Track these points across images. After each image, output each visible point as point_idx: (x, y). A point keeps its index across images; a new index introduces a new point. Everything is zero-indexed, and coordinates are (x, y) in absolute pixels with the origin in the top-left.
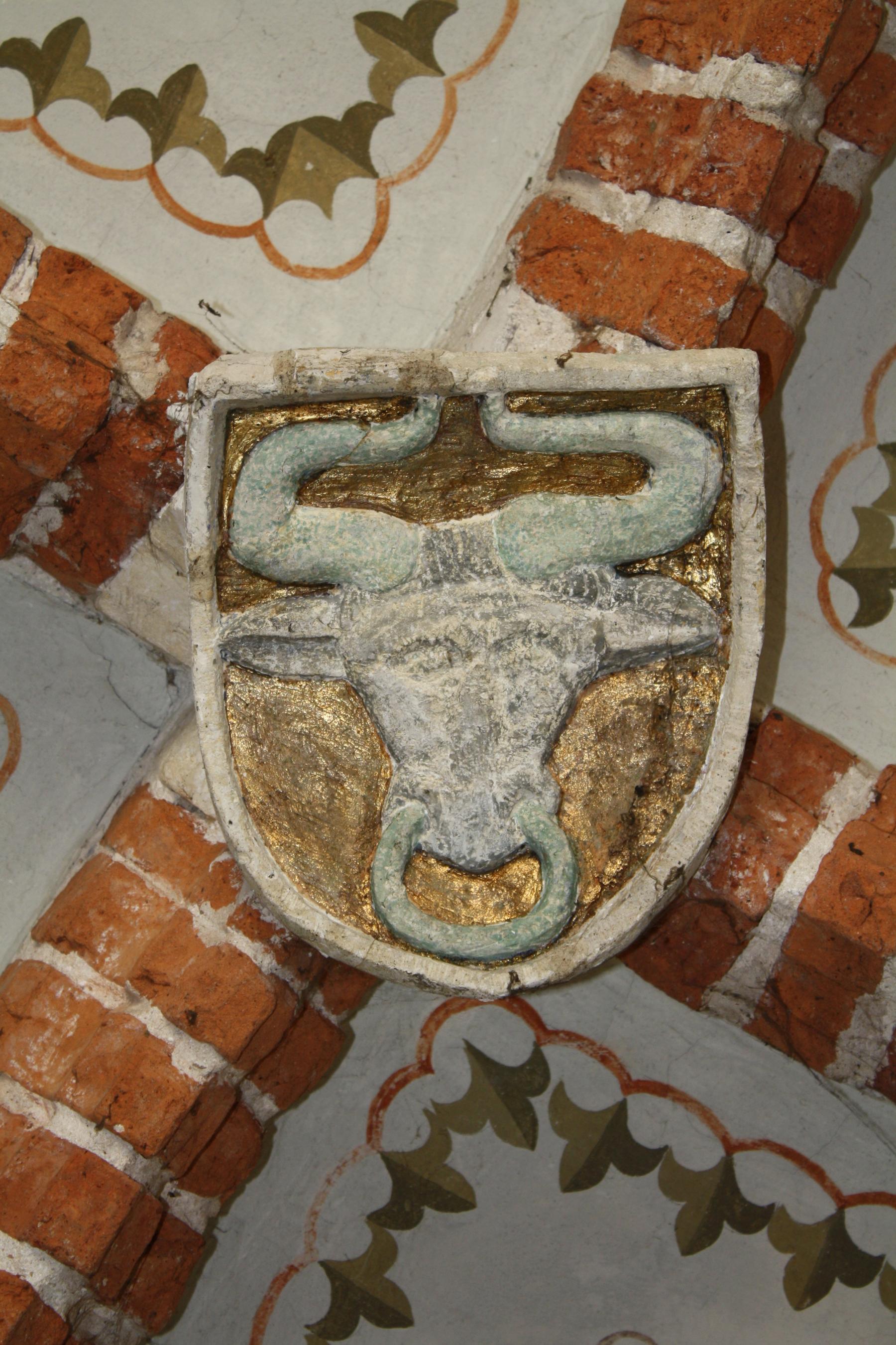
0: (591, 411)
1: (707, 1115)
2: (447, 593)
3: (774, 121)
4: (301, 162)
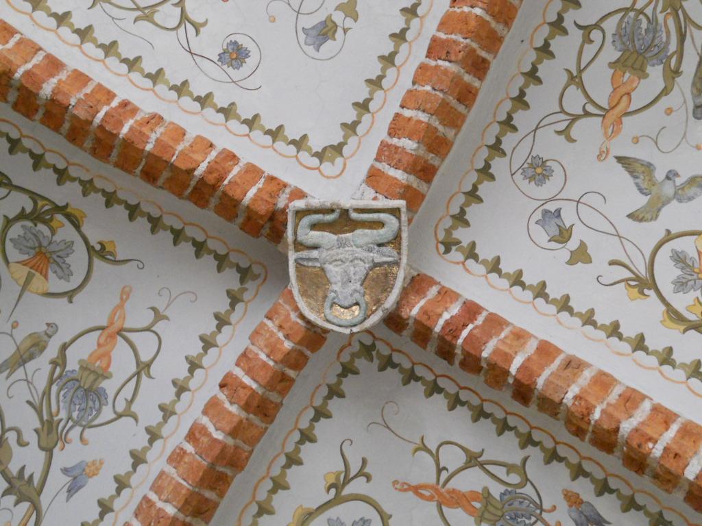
0: (371, 213)
2: (341, 250)
3: (413, 152)
4: (328, 154)
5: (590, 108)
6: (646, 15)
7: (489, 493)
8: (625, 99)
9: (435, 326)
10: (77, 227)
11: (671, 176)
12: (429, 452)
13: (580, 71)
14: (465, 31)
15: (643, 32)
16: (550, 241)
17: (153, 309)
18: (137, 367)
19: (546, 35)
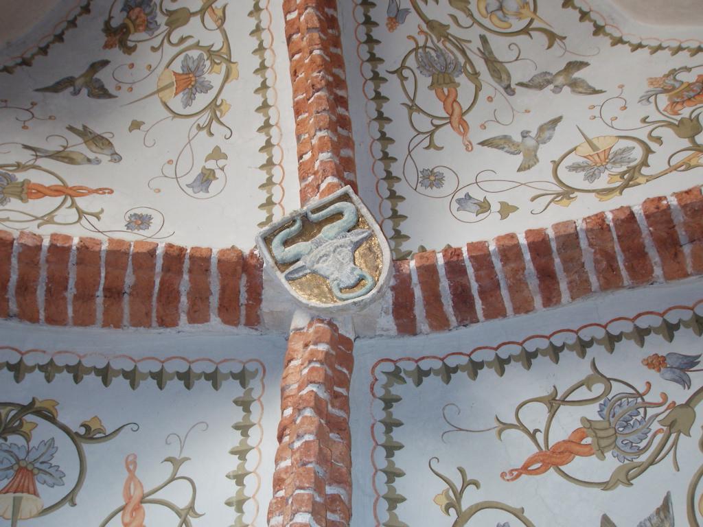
1: (435, 357)
5: (437, 122)
6: (429, 47)
7: (588, 421)
8: (455, 105)
9: (437, 262)
10: (52, 419)
11: (525, 135)
12: (511, 426)
13: (413, 101)
14: (316, 67)
15: (436, 58)
16: (477, 215)
17: (169, 460)
18: (180, 517)
19: (373, 87)
